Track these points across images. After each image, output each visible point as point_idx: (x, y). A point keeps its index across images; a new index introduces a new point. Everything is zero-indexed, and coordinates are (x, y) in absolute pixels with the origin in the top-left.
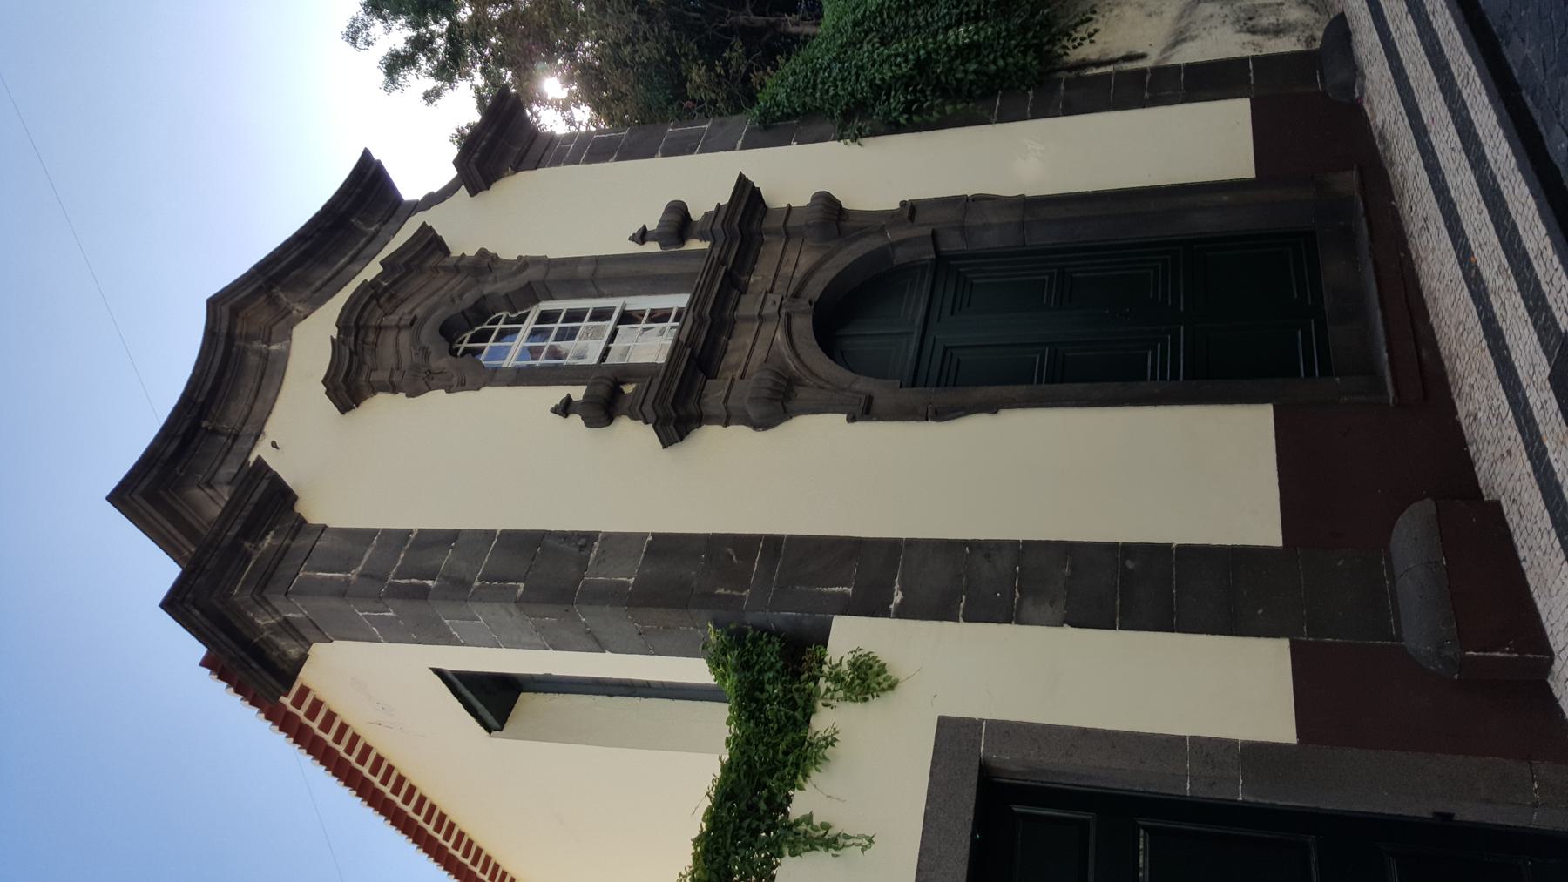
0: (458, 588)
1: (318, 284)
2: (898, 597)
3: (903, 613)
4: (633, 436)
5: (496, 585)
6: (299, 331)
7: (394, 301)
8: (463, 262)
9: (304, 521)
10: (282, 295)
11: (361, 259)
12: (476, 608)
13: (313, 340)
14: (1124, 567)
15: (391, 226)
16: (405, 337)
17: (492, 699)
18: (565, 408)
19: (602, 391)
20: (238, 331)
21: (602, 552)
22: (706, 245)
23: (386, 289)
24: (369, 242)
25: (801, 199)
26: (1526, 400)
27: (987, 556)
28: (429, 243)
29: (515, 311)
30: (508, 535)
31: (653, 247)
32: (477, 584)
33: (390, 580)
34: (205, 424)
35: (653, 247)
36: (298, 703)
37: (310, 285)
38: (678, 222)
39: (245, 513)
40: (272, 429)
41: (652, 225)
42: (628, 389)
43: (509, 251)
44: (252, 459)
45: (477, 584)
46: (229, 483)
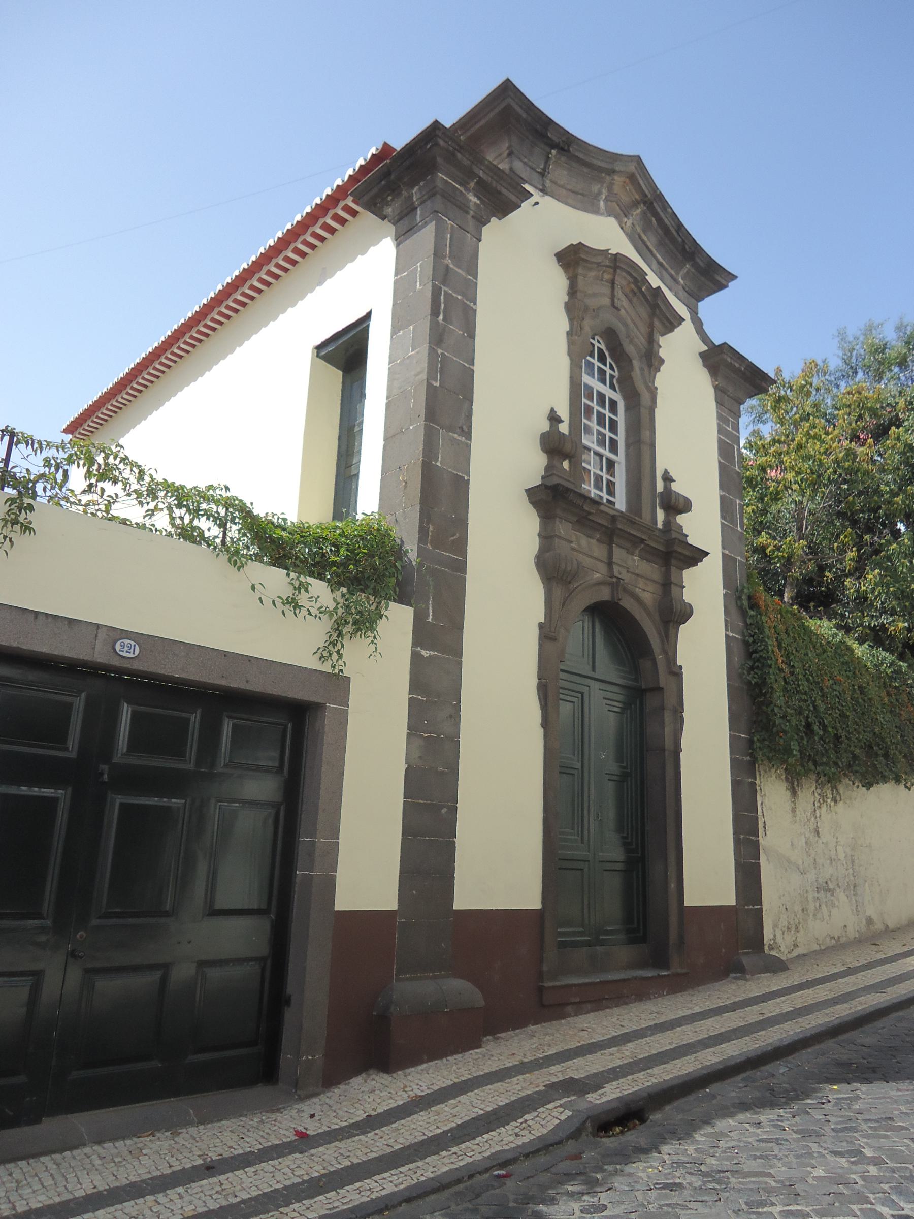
0: (437, 337)
1: (645, 238)
2: (425, 653)
3: (415, 656)
4: (532, 466)
5: (438, 365)
6: (612, 222)
7: (631, 295)
8: (656, 346)
9: (484, 225)
10: (639, 211)
11: (661, 271)
12: (424, 349)
13: (607, 234)
14: (444, 806)
15: (682, 294)
16: (606, 301)
17: (346, 353)
18: (554, 418)
19: (568, 447)
20: (616, 178)
21: (459, 443)
22: (660, 525)
23: (640, 289)
24: (672, 276)
25: (688, 596)
26: (554, 1065)
27: (451, 716)
28: (671, 323)
29: (619, 381)
30: (469, 375)
31: (660, 486)
32: (440, 351)
33: (444, 288)
34: (554, 152)
35: (660, 486)
36: (347, 209)
37: (644, 231)
38: (676, 505)
39: (494, 184)
40: (547, 202)
41: (674, 487)
42: (566, 465)
43: (661, 380)
44: (527, 187)
45: (440, 351)
46: (511, 169)
